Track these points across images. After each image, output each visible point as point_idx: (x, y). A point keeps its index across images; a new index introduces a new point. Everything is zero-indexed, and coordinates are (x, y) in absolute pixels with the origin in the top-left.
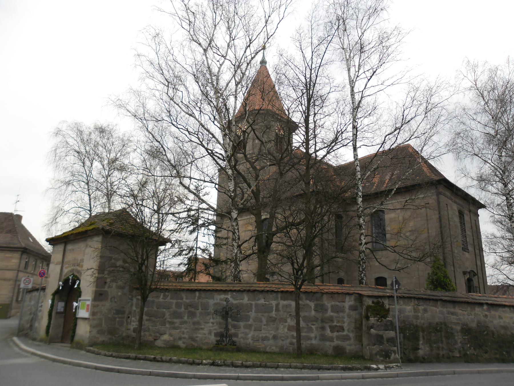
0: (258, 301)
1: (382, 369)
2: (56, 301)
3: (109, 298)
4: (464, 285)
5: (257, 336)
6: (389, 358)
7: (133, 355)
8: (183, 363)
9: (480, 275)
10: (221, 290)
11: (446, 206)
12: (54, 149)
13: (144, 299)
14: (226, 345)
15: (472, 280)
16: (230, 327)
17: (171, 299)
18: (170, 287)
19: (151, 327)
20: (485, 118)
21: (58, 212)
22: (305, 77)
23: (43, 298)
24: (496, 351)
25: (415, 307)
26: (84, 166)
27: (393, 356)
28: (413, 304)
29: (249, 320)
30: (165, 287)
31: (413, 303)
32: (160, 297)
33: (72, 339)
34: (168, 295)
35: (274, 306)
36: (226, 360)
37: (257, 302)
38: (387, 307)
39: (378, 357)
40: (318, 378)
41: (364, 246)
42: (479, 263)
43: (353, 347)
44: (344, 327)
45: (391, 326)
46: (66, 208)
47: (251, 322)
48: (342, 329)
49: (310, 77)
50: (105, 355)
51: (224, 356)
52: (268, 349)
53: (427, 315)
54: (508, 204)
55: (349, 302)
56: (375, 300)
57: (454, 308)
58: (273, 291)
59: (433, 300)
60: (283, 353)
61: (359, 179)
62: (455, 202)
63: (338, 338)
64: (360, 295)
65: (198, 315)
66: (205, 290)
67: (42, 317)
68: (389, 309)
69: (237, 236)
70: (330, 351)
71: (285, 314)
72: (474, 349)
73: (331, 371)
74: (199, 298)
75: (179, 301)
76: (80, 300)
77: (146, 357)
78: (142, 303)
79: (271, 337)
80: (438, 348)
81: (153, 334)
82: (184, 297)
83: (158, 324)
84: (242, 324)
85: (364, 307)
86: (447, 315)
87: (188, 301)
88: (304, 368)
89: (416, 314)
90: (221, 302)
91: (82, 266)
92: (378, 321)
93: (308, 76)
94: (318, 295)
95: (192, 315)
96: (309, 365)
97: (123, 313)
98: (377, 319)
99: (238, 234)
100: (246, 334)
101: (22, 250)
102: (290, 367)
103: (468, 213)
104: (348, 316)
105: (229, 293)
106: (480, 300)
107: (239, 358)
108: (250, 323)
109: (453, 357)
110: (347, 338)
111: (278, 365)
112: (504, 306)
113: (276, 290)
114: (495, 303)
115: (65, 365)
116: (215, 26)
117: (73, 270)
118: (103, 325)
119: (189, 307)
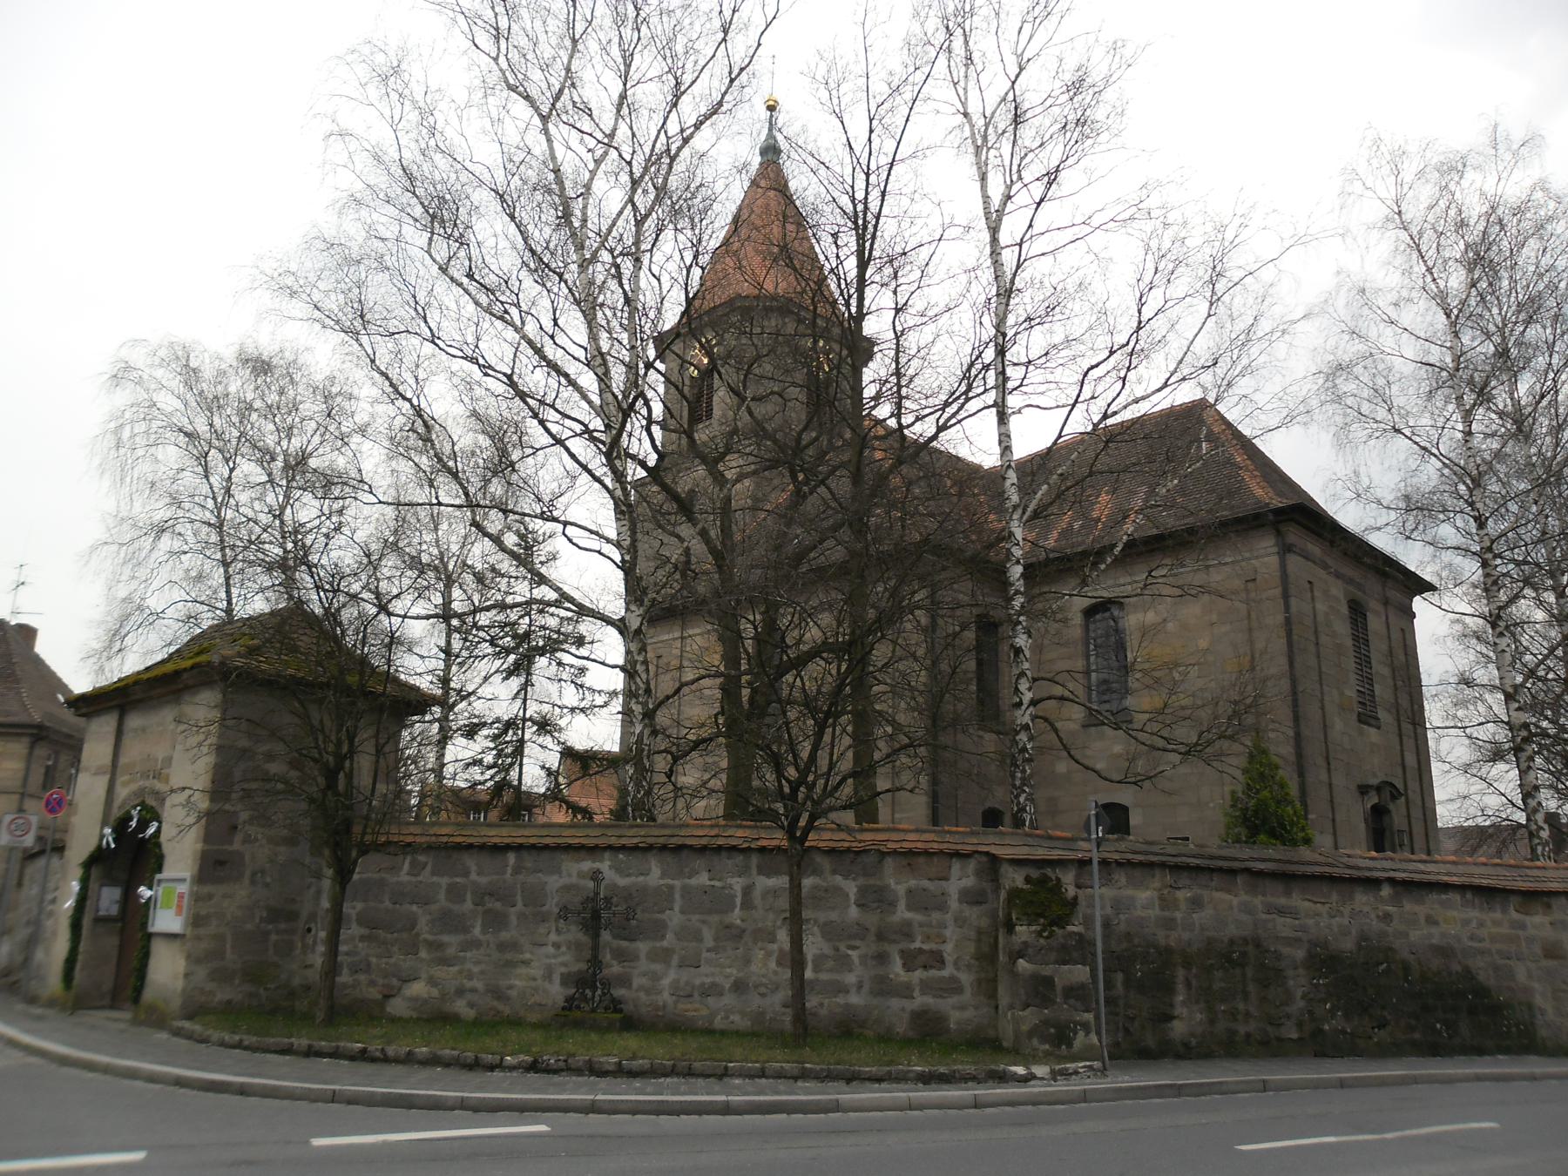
0: (689, 878)
1: (1042, 1079)
2: (93, 885)
3: (248, 873)
4: (1362, 826)
5: (687, 983)
6: (1070, 1045)
7: (301, 1042)
8: (447, 1064)
9: (1414, 796)
10: (582, 847)
11: (1308, 586)
12: (112, 425)
13: (343, 875)
14: (593, 1011)
15: (1389, 812)
16: (607, 957)
17: (433, 873)
18: (418, 839)
19: (374, 960)
20: (1427, 318)
21: (126, 617)
22: (853, 199)
23: (58, 876)
24: (1413, 1022)
25: (1165, 892)
26: (207, 477)
27: (1080, 1040)
28: (1157, 884)
29: (663, 937)
30: (402, 838)
31: (1158, 880)
32: (401, 869)
33: (136, 998)
34: (426, 864)
35: (739, 894)
36: (574, 1055)
37: (687, 881)
38: (1071, 891)
39: (1035, 1042)
40: (836, 1107)
41: (1028, 712)
42: (1411, 759)
43: (969, 1014)
44: (945, 955)
45: (1079, 950)
46: (155, 603)
47: (669, 940)
48: (938, 960)
49: (866, 198)
50: (222, 1044)
51: (577, 1046)
52: (718, 1023)
53: (1203, 917)
54: (1489, 581)
55: (961, 879)
56: (1035, 873)
57: (1288, 894)
58: (734, 848)
59: (1220, 870)
60: (760, 1033)
61: (1015, 507)
62: (1338, 575)
63: (926, 987)
64: (994, 860)
65: (514, 920)
66: (533, 847)
67: (54, 933)
68: (1076, 898)
69: (642, 685)
70: (901, 1028)
71: (771, 916)
72: (1347, 1016)
73: (884, 1085)
74: (517, 870)
75: (458, 880)
76: (160, 881)
77: (338, 1047)
78: (338, 888)
79: (727, 986)
80: (1233, 1015)
81: (381, 981)
82: (474, 868)
83: (395, 949)
84: (642, 947)
85: (1003, 895)
86: (1264, 916)
87: (483, 880)
88: (804, 1075)
89: (1167, 914)
90: (583, 882)
91: (167, 781)
92: (1041, 936)
93: (860, 195)
94: (869, 860)
95: (495, 921)
96: (818, 1067)
97: (292, 916)
98: (1039, 928)
99: (644, 676)
100: (656, 977)
101: (35, 731)
102: (762, 1074)
103: (1380, 608)
104: (956, 920)
105: (607, 855)
106: (1370, 869)
107: (614, 1049)
108: (665, 943)
109: (1280, 1040)
110: (953, 987)
111: (726, 1068)
112: (1445, 887)
113: (745, 845)
114: (1417, 877)
115: (91, 1075)
116: (574, 41)
117: (142, 790)
118: (229, 954)
119: (486, 898)
